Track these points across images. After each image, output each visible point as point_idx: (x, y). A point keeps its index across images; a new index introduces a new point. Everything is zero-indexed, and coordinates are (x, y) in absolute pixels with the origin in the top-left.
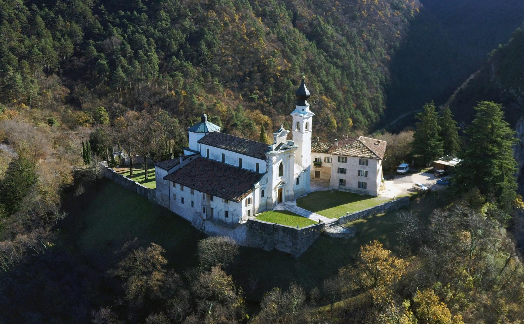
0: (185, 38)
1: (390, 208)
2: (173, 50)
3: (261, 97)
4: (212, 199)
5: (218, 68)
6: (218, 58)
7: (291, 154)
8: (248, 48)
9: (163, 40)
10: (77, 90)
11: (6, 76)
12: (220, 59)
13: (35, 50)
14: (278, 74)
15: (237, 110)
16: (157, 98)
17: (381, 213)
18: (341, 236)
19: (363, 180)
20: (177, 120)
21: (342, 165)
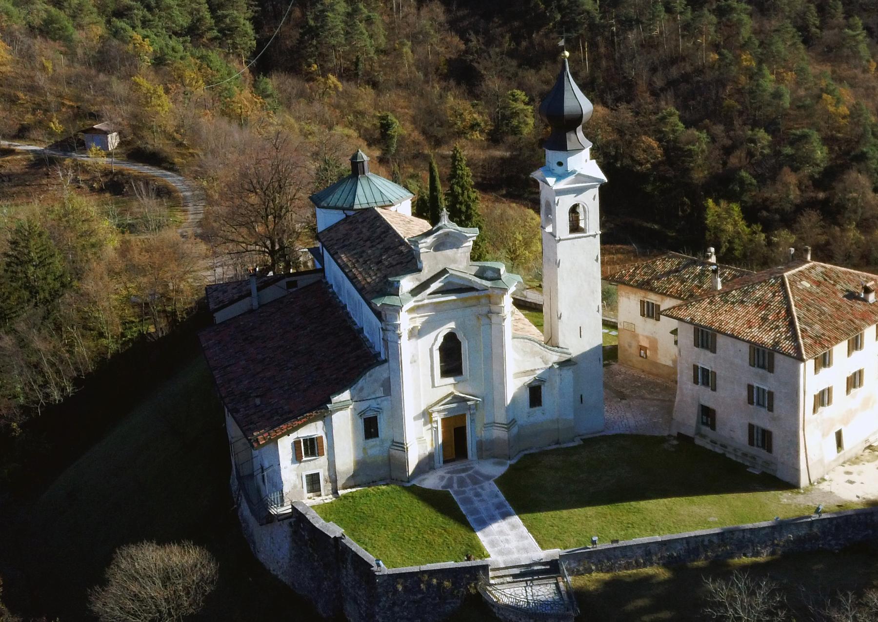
1: (799, 540)
4: (675, 362)
7: (494, 308)
10: (475, 42)
16: (674, 72)
17: (757, 554)
19: (762, 419)
21: (705, 359)
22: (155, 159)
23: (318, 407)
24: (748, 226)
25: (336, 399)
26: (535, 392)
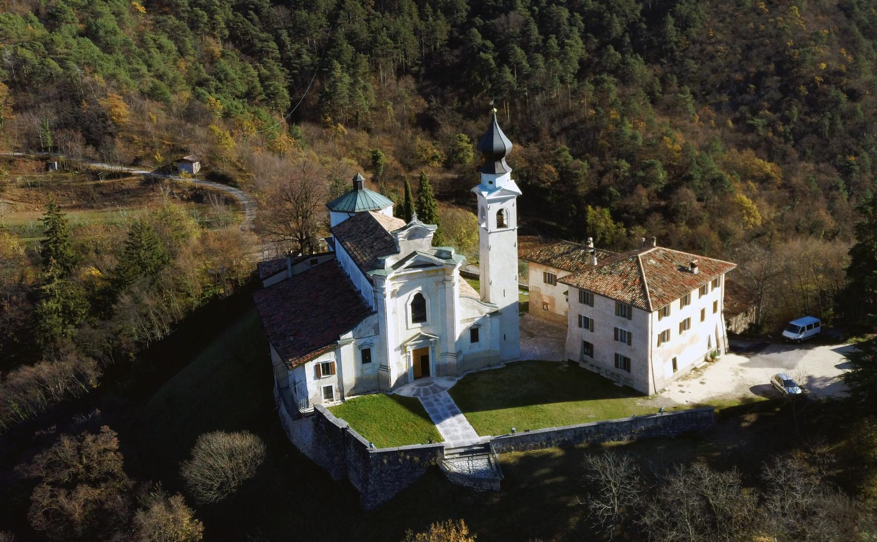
0: (642, 12)
1: (648, 430)
2: (614, 34)
3: (771, 125)
5: (693, 66)
6: (698, 47)
7: (447, 277)
8: (762, 27)
9: (600, 15)
10: (435, 103)
11: (328, 78)
12: (702, 51)
13: (384, 36)
14: (818, 79)
15: (706, 149)
16: (566, 122)
18: (466, 484)
19: (624, 350)
20: (585, 164)
21: (586, 311)
22: (224, 179)
23: (332, 343)
24: (615, 224)
25: (343, 337)
26: (474, 333)
